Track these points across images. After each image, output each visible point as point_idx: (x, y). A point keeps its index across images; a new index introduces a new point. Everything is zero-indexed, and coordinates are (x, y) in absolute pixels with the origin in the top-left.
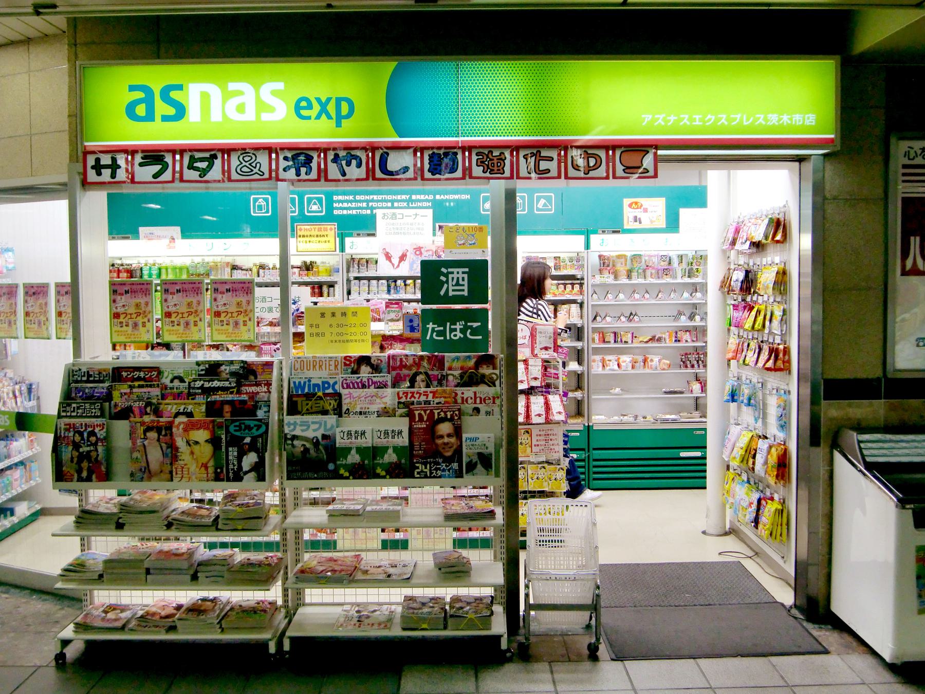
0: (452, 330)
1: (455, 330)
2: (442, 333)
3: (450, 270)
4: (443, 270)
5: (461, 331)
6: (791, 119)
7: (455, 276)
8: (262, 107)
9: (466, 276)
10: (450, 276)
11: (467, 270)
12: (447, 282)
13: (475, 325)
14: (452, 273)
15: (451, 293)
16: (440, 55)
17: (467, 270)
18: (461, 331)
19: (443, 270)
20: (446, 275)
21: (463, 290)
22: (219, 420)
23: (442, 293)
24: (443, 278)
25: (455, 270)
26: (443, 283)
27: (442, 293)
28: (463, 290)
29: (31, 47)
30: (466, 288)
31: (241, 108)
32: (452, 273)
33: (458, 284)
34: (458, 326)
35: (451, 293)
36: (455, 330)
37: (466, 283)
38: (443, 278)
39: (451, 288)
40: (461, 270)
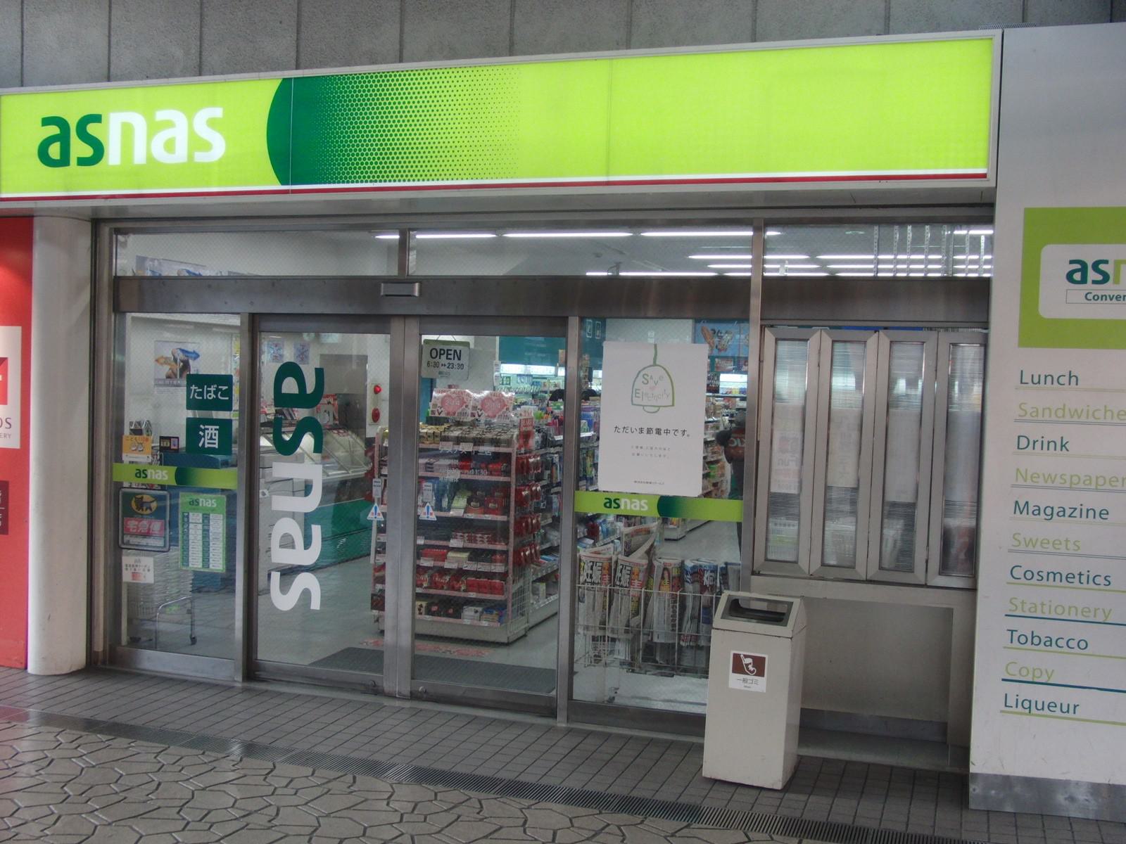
0: (208, 392)
1: (210, 392)
2: (201, 394)
3: (206, 427)
4: (202, 427)
5: (216, 393)
6: (949, 262)
7: (210, 432)
8: (641, 507)
9: (217, 432)
10: (207, 432)
11: (218, 427)
12: (204, 436)
13: (224, 388)
14: (208, 429)
15: (207, 446)
16: (227, 553)
17: (218, 427)
18: (216, 393)
19: (202, 427)
20: (204, 431)
21: (215, 444)
22: (180, 563)
23: (200, 445)
24: (201, 433)
25: (210, 427)
26: (200, 437)
27: (200, 445)
28: (215, 444)
29: (140, 617)
30: (217, 442)
31: (635, 506)
32: (208, 429)
33: (211, 439)
34: (212, 389)
35: (207, 446)
36: (210, 392)
37: (217, 438)
38: (201, 433)
39: (207, 441)
40: (214, 427)
